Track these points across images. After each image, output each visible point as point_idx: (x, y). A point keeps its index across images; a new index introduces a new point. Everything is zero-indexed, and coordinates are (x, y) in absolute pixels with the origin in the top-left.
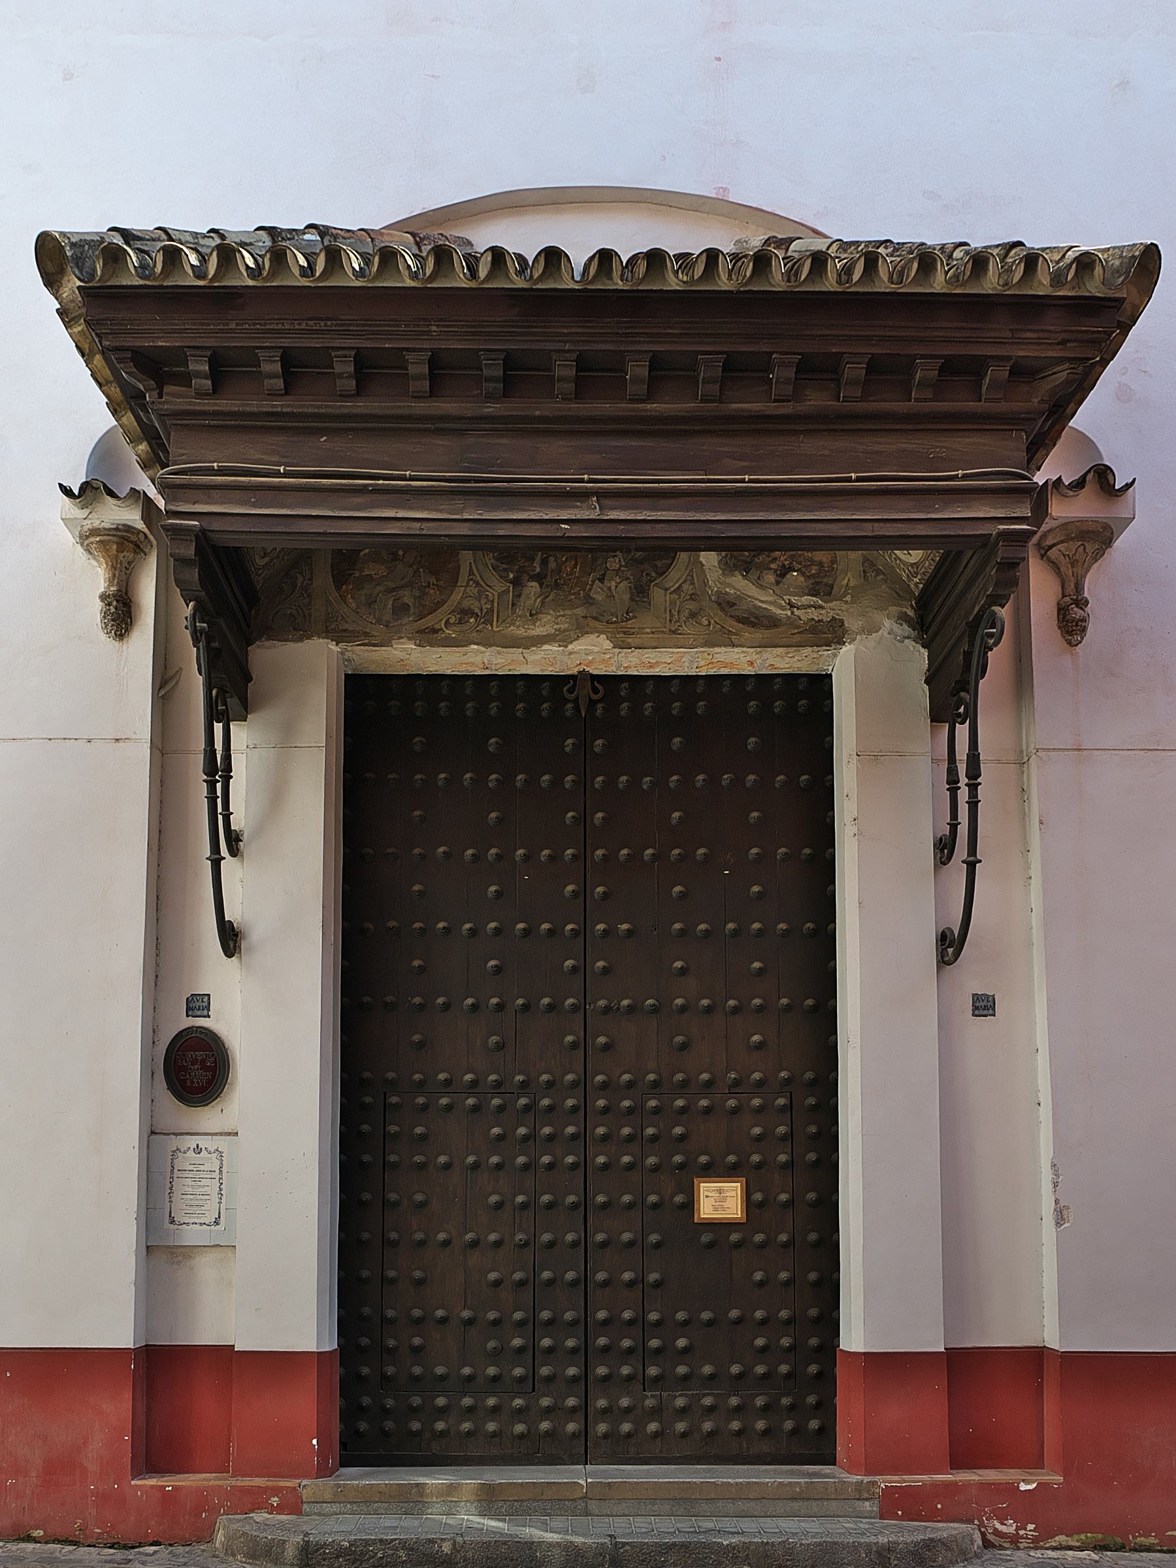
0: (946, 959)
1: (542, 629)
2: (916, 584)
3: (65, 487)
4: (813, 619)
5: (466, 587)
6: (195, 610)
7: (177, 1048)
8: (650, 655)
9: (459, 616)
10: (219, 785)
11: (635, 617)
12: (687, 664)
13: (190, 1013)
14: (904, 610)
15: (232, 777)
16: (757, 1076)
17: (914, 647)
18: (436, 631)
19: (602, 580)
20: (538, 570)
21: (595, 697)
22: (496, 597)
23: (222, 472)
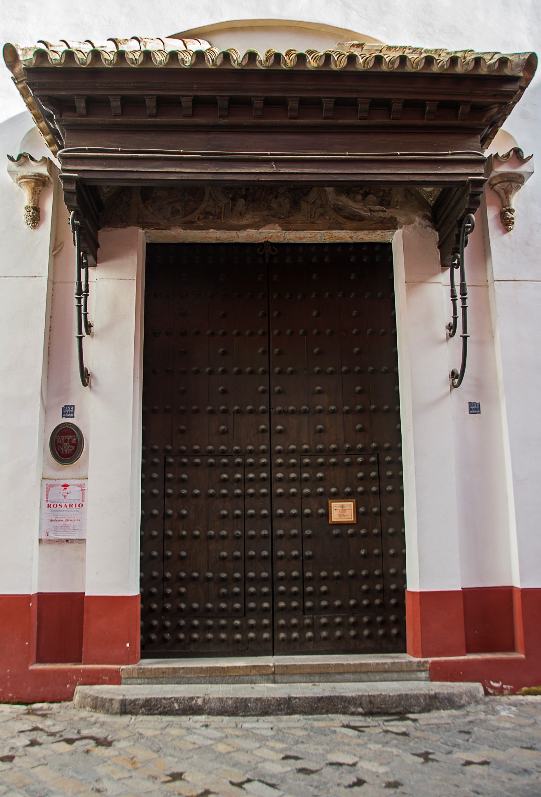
0: (455, 385)
1: (246, 221)
2: (431, 201)
3: (10, 156)
4: (381, 217)
5: (208, 201)
6: (74, 215)
7: (56, 434)
8: (300, 234)
9: (204, 215)
10: (83, 300)
11: (292, 216)
12: (319, 238)
13: (64, 415)
14: (426, 213)
15: (88, 295)
16: (360, 446)
17: (432, 231)
18: (192, 222)
19: (276, 198)
20: (244, 193)
21: (273, 254)
22: (223, 206)
23: (90, 151)
